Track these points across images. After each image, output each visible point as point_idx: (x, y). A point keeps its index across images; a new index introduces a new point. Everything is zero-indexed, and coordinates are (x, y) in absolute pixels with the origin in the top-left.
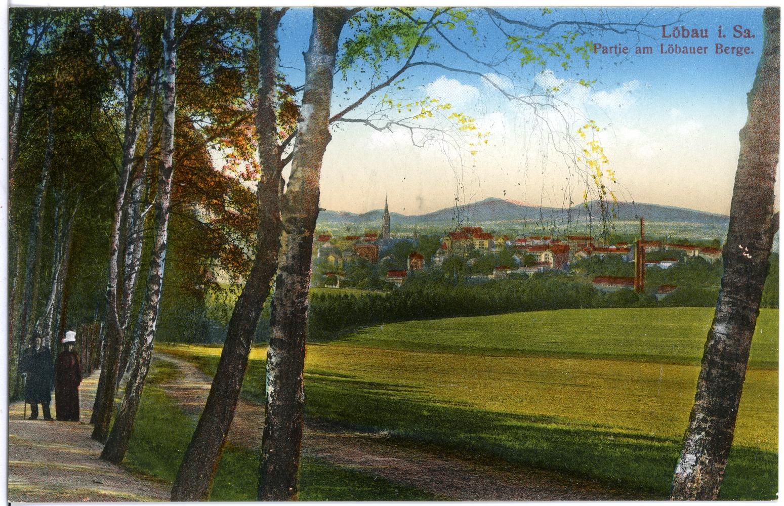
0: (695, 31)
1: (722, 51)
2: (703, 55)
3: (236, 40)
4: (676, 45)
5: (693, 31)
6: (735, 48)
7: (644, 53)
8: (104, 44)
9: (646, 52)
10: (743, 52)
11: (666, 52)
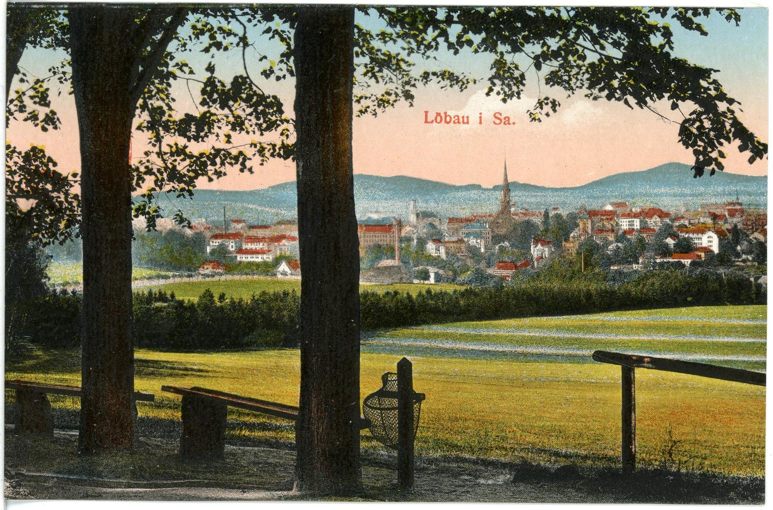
0: (456, 118)
5: (454, 117)
8: (57, 11)
11: (432, 122)
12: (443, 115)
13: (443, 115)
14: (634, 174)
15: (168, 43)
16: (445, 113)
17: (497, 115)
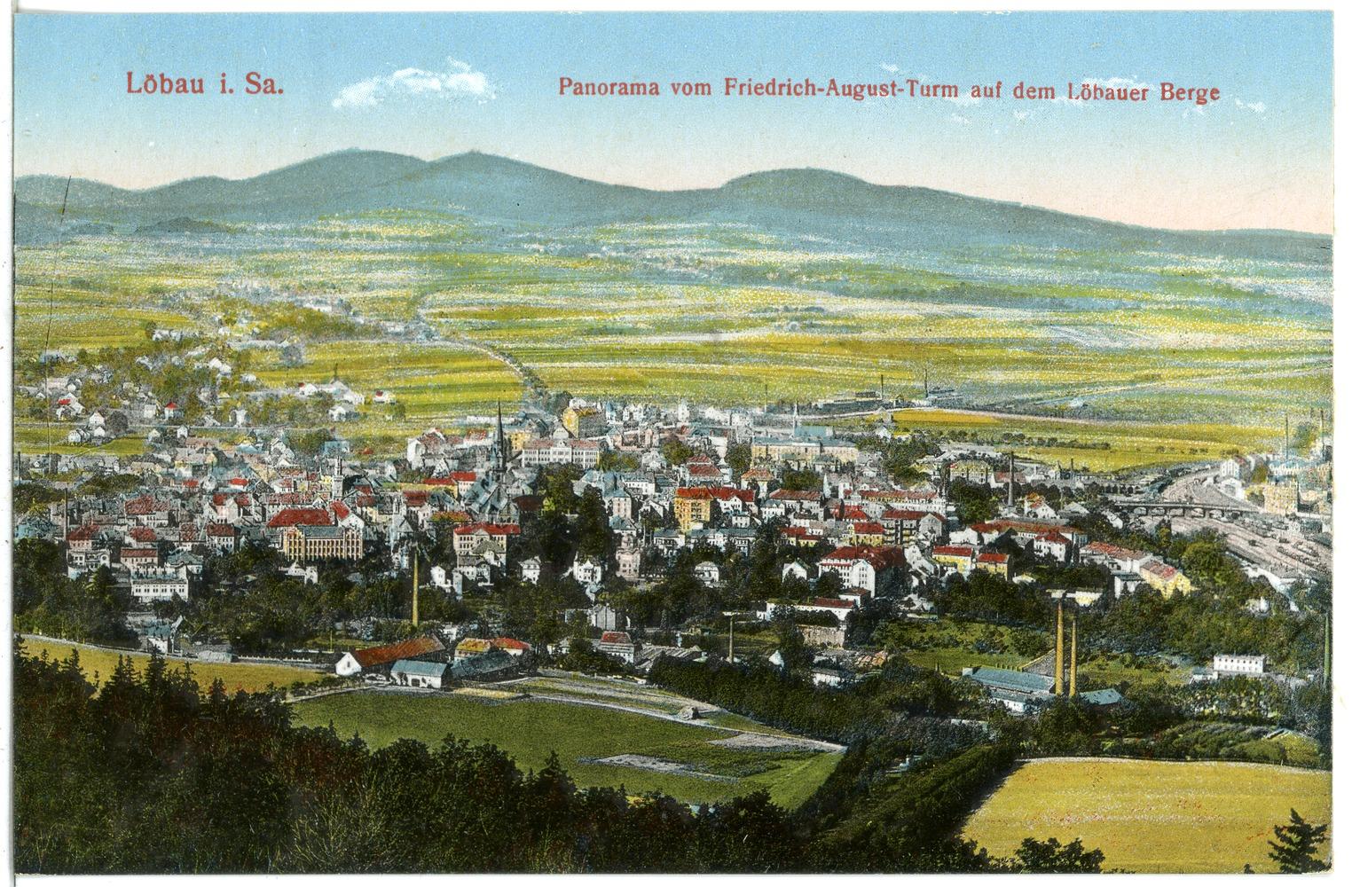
0: (181, 83)
1: (1172, 97)
2: (993, 101)
3: (21, 339)
4: (162, 76)
5: (178, 82)
6: (1193, 90)
7: (632, 93)
9: (636, 91)
10: (1208, 97)
11: (140, 91)
12: (1091, 88)
13: (158, 80)
14: (517, 164)
15: (142, 196)
16: (162, 76)
17: (253, 78)
